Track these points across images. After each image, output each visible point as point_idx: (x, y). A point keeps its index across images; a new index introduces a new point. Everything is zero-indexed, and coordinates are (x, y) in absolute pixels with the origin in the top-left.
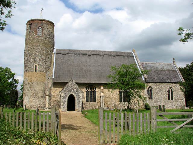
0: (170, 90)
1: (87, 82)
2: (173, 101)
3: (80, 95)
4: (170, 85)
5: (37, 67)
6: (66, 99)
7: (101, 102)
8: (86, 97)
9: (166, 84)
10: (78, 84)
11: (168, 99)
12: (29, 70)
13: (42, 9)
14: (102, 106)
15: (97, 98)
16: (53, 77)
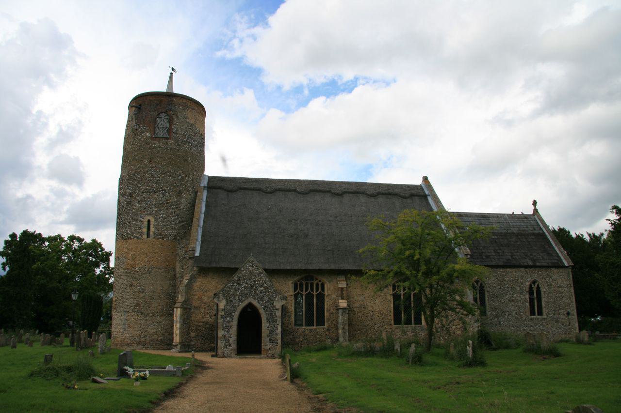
0: (535, 288)
1: (288, 268)
2: (544, 319)
3: (277, 307)
4: (535, 275)
5: (152, 226)
6: (232, 317)
7: (341, 327)
8: (293, 312)
9: (523, 269)
10: (270, 272)
11: (528, 313)
12: (128, 234)
13: (173, 69)
14: (341, 339)
15: (326, 314)
16: (197, 254)
